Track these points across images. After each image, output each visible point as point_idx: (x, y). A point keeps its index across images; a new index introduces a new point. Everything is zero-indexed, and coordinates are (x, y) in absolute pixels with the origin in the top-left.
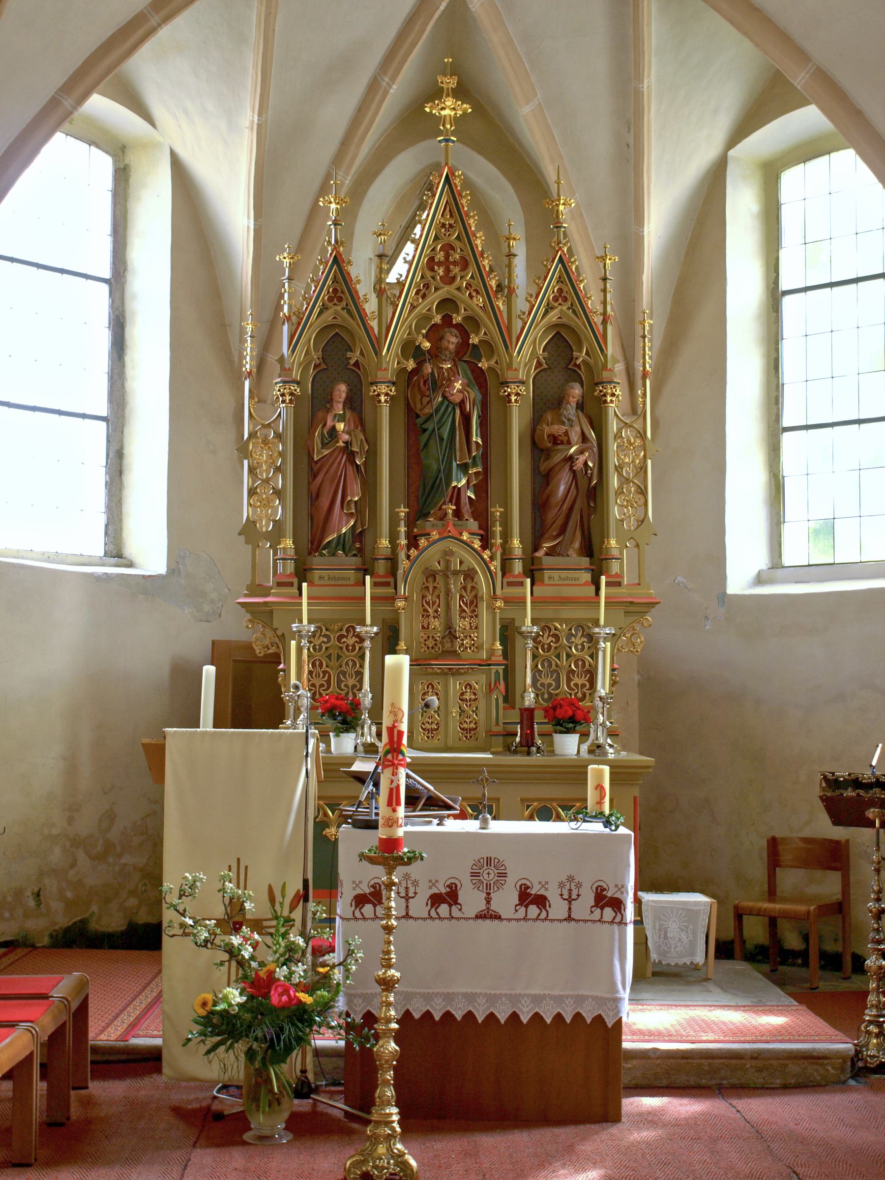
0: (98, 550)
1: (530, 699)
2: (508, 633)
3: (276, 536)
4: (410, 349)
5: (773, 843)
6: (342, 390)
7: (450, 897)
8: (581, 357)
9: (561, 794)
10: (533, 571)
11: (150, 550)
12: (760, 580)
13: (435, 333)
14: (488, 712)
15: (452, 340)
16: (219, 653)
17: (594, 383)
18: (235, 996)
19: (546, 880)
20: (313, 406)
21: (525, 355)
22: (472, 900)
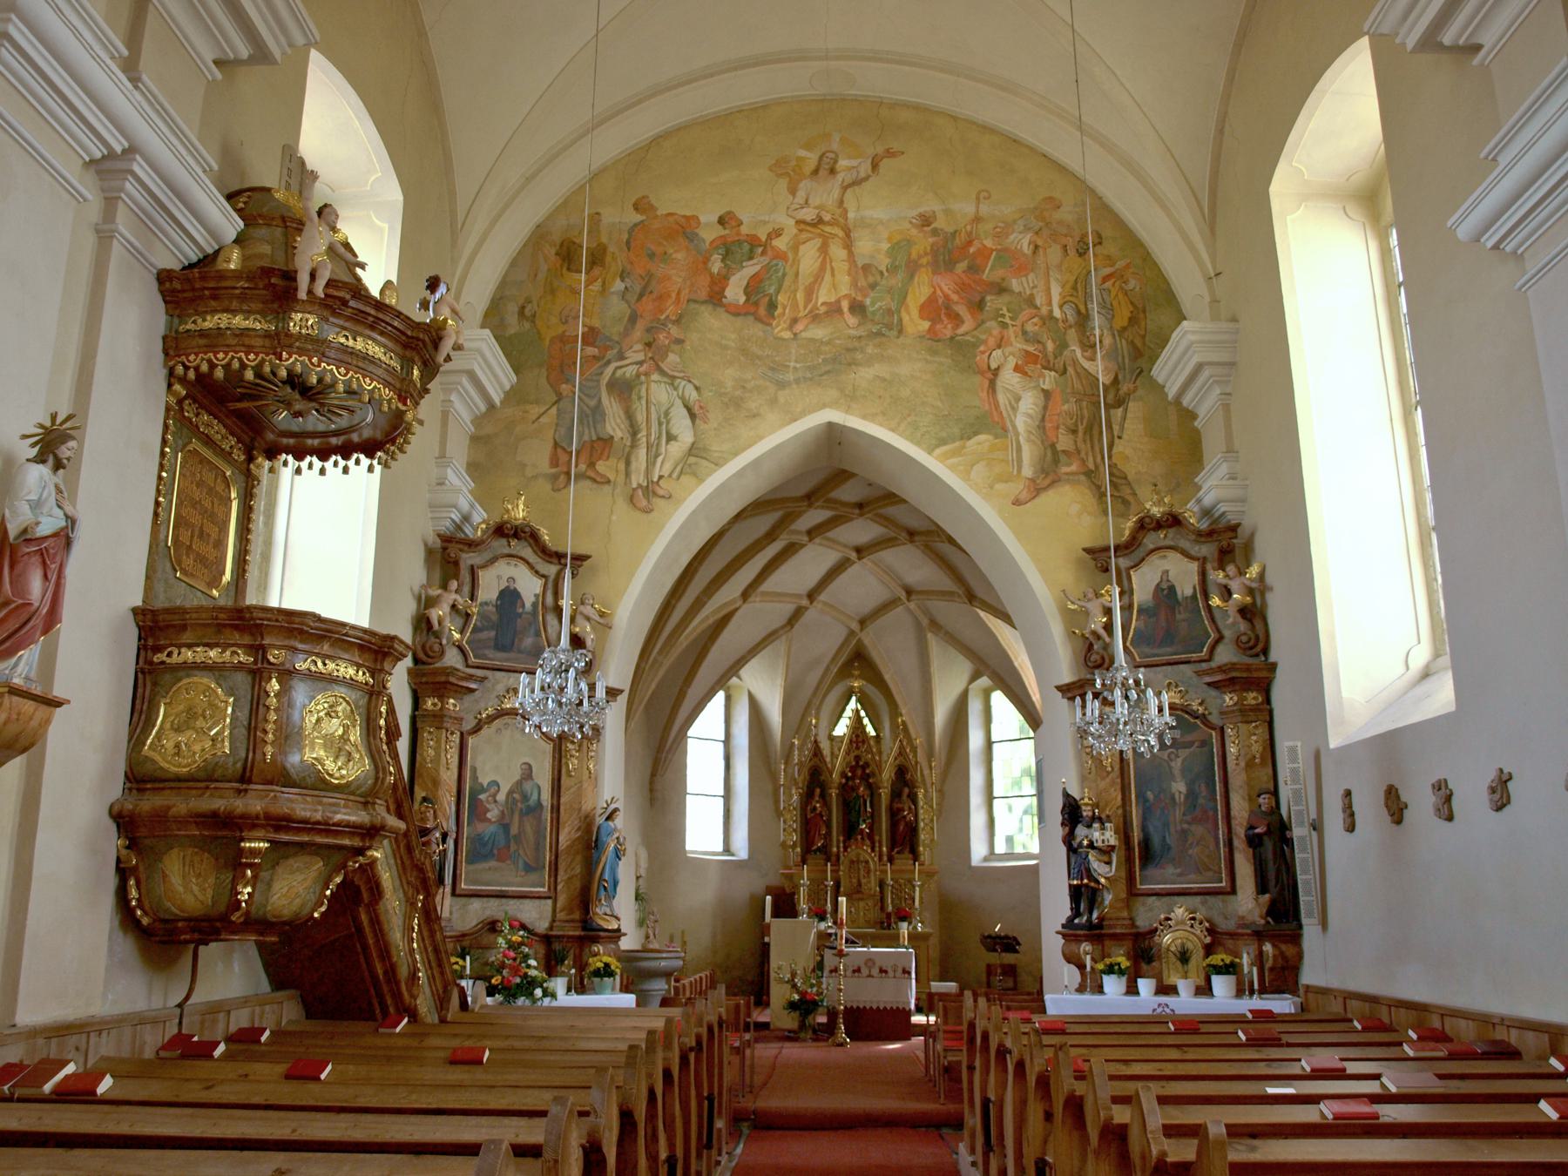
0: (720, 849)
1: (890, 908)
2: (882, 884)
3: (794, 846)
4: (843, 775)
5: (989, 966)
6: (818, 791)
7: (858, 970)
8: (908, 777)
9: (894, 940)
10: (891, 860)
11: (741, 850)
12: (986, 859)
13: (853, 769)
14: (874, 914)
15: (859, 772)
16: (769, 891)
17: (911, 785)
18: (797, 997)
19: (888, 966)
20: (808, 797)
21: (887, 775)
22: (865, 971)
